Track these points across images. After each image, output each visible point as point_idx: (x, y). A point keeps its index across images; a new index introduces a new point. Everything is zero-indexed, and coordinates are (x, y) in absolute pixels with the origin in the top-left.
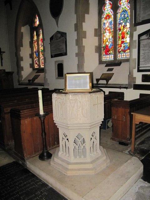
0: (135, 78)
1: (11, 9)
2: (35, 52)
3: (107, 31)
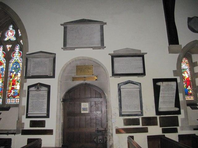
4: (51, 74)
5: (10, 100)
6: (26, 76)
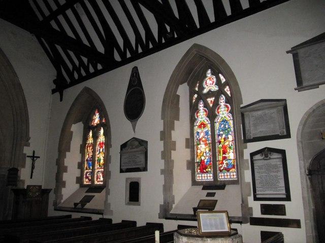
0: (251, 208)
1: (61, 100)
2: (87, 160)
3: (202, 143)
4: (284, 132)
5: (223, 174)
6: (244, 138)
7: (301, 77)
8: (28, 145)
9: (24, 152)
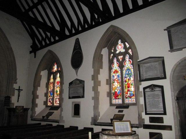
0: (144, 119)
1: (35, 57)
2: (50, 92)
3: (115, 82)
7: (172, 44)
8: (16, 83)
9: (14, 87)
